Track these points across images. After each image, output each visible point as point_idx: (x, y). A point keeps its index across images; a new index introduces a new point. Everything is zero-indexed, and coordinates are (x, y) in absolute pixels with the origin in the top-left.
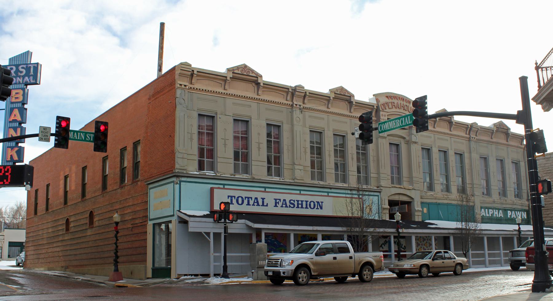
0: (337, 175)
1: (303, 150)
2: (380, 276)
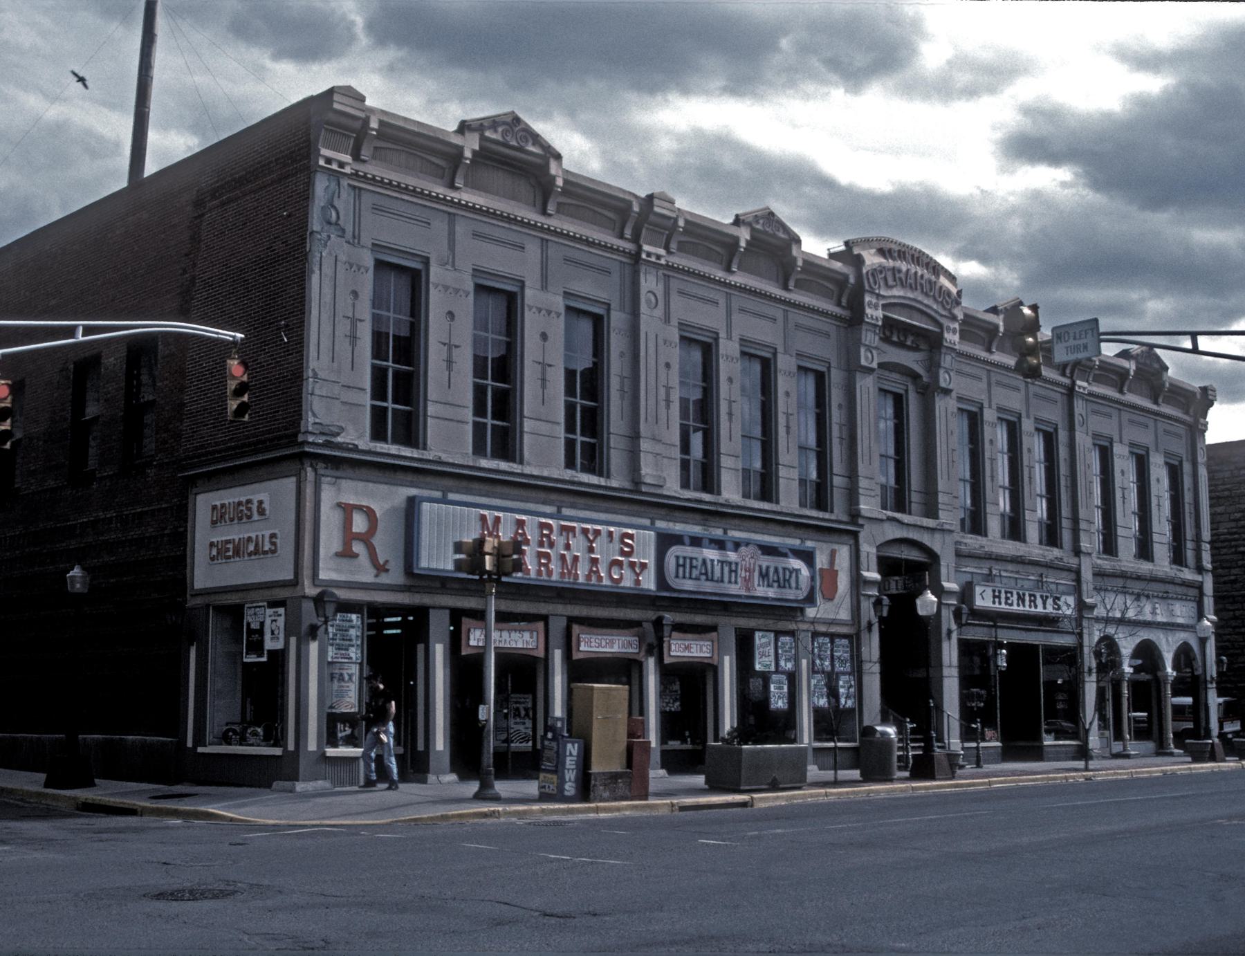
0: (479, 429)
1: (343, 328)
2: (1014, 773)
